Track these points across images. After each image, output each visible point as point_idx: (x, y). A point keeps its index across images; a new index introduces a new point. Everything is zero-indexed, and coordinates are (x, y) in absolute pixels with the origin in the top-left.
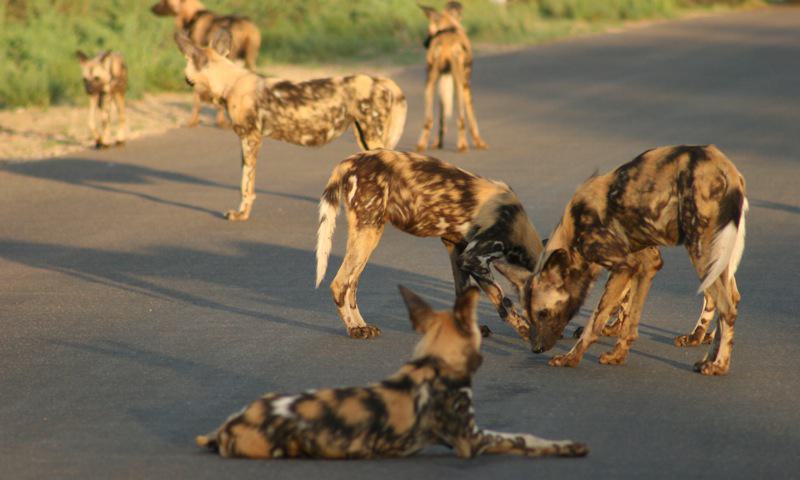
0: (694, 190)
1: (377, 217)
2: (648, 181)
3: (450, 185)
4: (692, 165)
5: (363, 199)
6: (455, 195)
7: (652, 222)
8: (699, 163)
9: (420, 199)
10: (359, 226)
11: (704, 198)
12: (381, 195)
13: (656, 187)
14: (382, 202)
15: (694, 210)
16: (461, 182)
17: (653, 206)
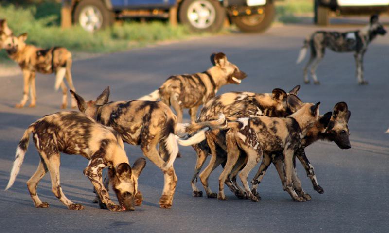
0: (150, 123)
1: (54, 149)
2: (131, 117)
3: (79, 125)
4: (151, 111)
5: (44, 143)
6: (82, 131)
7: (131, 134)
8: (154, 110)
9: (66, 134)
10: (48, 157)
11: (154, 126)
12: (52, 138)
13: (134, 120)
14: (54, 141)
15: (148, 132)
16: (85, 124)
17: (132, 128)
